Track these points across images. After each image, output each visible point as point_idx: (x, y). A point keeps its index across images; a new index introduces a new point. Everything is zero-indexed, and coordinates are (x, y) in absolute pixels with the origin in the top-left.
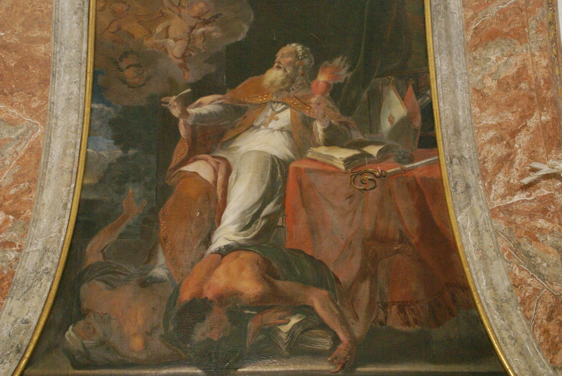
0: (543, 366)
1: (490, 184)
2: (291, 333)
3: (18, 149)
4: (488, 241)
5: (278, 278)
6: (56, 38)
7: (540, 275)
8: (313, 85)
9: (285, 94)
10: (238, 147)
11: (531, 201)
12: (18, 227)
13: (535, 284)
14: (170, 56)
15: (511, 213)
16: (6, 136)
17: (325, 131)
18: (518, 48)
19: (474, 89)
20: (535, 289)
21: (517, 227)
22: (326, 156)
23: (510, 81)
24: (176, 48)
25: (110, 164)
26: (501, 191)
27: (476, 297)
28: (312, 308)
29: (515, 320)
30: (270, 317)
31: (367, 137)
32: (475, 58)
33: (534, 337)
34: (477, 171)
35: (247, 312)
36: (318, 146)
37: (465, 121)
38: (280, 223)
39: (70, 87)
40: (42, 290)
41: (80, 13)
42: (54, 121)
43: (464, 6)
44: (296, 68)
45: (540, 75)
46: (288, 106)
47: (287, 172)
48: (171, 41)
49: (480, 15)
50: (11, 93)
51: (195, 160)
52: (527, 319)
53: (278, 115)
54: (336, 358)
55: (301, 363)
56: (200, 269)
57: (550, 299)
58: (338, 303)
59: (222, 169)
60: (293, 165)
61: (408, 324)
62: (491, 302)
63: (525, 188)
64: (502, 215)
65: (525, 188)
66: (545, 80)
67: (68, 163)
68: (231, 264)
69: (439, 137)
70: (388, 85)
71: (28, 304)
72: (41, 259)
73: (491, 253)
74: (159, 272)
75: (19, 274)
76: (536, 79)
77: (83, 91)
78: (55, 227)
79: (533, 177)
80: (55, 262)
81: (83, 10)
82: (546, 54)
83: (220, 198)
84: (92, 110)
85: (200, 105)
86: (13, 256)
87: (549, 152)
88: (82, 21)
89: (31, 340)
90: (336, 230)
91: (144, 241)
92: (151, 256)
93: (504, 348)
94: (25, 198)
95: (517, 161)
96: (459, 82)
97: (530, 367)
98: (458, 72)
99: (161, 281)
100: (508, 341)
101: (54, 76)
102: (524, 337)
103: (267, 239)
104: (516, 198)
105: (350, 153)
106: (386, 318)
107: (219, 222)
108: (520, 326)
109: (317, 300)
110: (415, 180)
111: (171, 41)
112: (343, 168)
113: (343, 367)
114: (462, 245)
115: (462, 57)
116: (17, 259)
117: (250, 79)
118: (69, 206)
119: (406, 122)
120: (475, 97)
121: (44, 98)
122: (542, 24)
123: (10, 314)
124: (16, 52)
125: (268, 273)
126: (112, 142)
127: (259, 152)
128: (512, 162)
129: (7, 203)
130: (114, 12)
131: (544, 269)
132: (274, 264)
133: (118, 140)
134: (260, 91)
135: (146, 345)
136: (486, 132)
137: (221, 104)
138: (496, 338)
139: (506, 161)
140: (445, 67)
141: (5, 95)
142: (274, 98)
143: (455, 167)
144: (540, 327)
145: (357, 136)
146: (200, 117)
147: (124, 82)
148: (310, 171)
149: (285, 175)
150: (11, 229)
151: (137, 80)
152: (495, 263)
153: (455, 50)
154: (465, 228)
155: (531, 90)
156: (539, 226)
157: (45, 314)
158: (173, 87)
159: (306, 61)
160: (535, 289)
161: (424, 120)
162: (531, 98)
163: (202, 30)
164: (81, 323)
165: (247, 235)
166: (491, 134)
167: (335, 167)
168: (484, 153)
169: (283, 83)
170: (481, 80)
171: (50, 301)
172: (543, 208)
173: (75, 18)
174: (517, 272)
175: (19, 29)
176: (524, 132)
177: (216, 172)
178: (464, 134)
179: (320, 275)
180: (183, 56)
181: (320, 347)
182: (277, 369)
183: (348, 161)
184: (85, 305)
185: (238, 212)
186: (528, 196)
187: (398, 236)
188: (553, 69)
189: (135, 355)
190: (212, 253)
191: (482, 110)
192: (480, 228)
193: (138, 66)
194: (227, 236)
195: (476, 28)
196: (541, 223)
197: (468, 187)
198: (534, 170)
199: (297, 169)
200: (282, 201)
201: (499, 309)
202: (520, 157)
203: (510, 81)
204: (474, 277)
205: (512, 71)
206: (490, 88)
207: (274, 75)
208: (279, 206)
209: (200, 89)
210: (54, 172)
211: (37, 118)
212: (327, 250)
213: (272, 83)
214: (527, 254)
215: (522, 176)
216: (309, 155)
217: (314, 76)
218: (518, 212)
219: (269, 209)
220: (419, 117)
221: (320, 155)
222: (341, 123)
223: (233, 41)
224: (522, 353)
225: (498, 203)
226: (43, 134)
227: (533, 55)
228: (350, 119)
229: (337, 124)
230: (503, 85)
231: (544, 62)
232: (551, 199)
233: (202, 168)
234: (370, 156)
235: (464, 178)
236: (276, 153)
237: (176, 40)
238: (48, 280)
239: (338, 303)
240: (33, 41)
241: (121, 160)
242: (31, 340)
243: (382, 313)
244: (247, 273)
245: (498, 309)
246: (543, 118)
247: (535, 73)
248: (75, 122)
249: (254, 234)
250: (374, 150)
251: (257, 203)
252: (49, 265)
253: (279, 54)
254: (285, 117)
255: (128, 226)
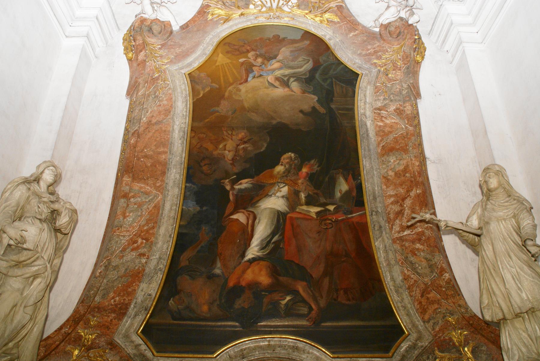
0: (418, 321)
1: (392, 225)
2: (286, 304)
3: (149, 207)
4: (391, 256)
5: (280, 276)
6: (170, 151)
7: (418, 273)
8: (300, 174)
9: (285, 178)
10: (260, 206)
11: (413, 234)
12: (147, 246)
13: (415, 278)
14: (226, 159)
15: (403, 241)
16: (144, 200)
17: (305, 197)
18: (404, 156)
19: (383, 176)
20: (415, 281)
21: (406, 248)
22: (306, 211)
23: (401, 172)
24: (229, 155)
25: (194, 214)
26: (398, 229)
27: (385, 285)
28: (298, 292)
29: (405, 297)
30: (276, 296)
31: (328, 201)
32: (383, 161)
33: (414, 306)
34: (385, 219)
35: (263, 293)
36: (302, 205)
37: (379, 193)
38: (281, 246)
39: (175, 175)
40: (158, 279)
41: (182, 139)
42: (167, 192)
43: (377, 135)
44: (291, 165)
45: (415, 170)
46: (286, 184)
47: (286, 219)
48: (227, 152)
49: (385, 140)
50: (148, 179)
51: (238, 212)
52: (411, 296)
53: (282, 189)
54: (310, 318)
55: (291, 321)
56: (239, 270)
57: (423, 286)
58: (312, 289)
59: (251, 217)
60: (289, 215)
61: (349, 300)
62: (392, 288)
63: (408, 227)
64: (398, 242)
65: (408, 227)
66: (418, 172)
67: (172, 214)
68: (255, 267)
69: (365, 201)
70: (338, 174)
71: (151, 286)
72: (158, 263)
73: (393, 262)
74: (217, 271)
75: (147, 270)
76: (414, 172)
77: (182, 177)
78: (165, 246)
79: (413, 221)
80: (164, 265)
81: (184, 138)
82: (418, 159)
83: (250, 233)
84: (186, 187)
85: (241, 184)
86: (144, 261)
87: (421, 209)
88: (183, 143)
89: (152, 304)
90: (312, 249)
91: (210, 255)
92: (214, 262)
93: (399, 312)
94: (151, 232)
95: (406, 214)
96: (375, 173)
97: (412, 321)
98: (375, 168)
99: (218, 276)
100: (401, 308)
101: (168, 170)
102: (409, 306)
103: (274, 252)
104: (405, 233)
105: (319, 209)
106: (337, 297)
107: (249, 245)
108: (407, 300)
109: (301, 287)
110: (353, 223)
111: (227, 152)
112: (315, 217)
113: (314, 323)
114: (378, 257)
115: (376, 160)
116: (146, 262)
117: (267, 171)
118: (172, 236)
119: (348, 193)
120: (384, 180)
121: (163, 181)
122: (415, 145)
123: (142, 290)
124: (151, 159)
125: (274, 272)
126: (195, 203)
127: (271, 208)
128: (403, 214)
129: (142, 234)
130: (199, 138)
131: (419, 269)
132: (278, 268)
133: (198, 202)
134: (272, 176)
135: (210, 309)
136: (389, 198)
137: (251, 183)
138: (395, 307)
139: (400, 214)
140: (368, 165)
141: (145, 179)
142: (279, 181)
143: (374, 217)
144: (417, 300)
145: (322, 200)
146: (240, 190)
147: (202, 172)
148: (297, 218)
149: (285, 221)
150: (144, 247)
151: (209, 171)
152: (395, 267)
153: (372, 157)
154: (379, 249)
155: (412, 177)
156: (417, 247)
157: (159, 292)
158: (227, 175)
159: (296, 161)
160: (415, 281)
161: (357, 192)
162: (412, 182)
163: (243, 146)
164: (177, 297)
165: (264, 252)
166: (392, 199)
167: (312, 217)
168: (389, 209)
169: (284, 173)
170: (387, 172)
171: (162, 285)
172: (419, 238)
173: (180, 142)
174: (406, 272)
175: (153, 148)
176: (409, 198)
177: (248, 219)
178: (378, 199)
179: (302, 274)
180: (233, 159)
181: (301, 312)
182: (279, 324)
183: (318, 213)
184: (179, 288)
185: (259, 240)
186: (411, 232)
187: (344, 253)
188: (422, 167)
189: (204, 314)
190: (245, 262)
191: (387, 187)
192: (387, 249)
193: (210, 164)
194: (254, 253)
195: (383, 146)
196: (418, 246)
197: (380, 227)
198: (414, 218)
199: (291, 218)
200: (283, 234)
201: (397, 291)
202: (407, 211)
203: (401, 172)
204: (384, 275)
205: (402, 167)
206: (391, 176)
207: (279, 169)
208: (281, 237)
209: (241, 176)
210: (166, 219)
211: (159, 191)
212: (306, 261)
213: (278, 173)
214: (411, 262)
215: (408, 221)
216: (297, 210)
217: (300, 169)
218: (406, 240)
219: (276, 238)
220: (355, 190)
221: (303, 210)
222: (314, 193)
223: (258, 151)
224: (408, 315)
225: (396, 235)
226: (161, 199)
227: (411, 160)
228: (319, 192)
229: (312, 194)
230: (397, 174)
231: (417, 164)
232: (423, 233)
233: (241, 217)
234: (330, 210)
235: (379, 223)
236: (280, 209)
237: (229, 151)
238: (161, 274)
239: (312, 289)
240: (160, 153)
241: (199, 212)
242: (152, 304)
243: (335, 294)
244: (263, 272)
245: (396, 292)
246: (418, 191)
247: (413, 169)
248: (177, 193)
249: (267, 252)
250: (331, 208)
251: (268, 236)
252: (162, 266)
253: (282, 158)
254: (285, 190)
255: (202, 247)
